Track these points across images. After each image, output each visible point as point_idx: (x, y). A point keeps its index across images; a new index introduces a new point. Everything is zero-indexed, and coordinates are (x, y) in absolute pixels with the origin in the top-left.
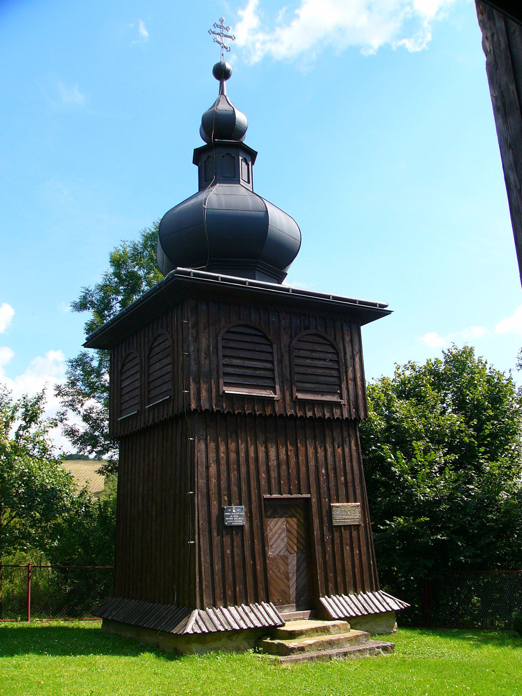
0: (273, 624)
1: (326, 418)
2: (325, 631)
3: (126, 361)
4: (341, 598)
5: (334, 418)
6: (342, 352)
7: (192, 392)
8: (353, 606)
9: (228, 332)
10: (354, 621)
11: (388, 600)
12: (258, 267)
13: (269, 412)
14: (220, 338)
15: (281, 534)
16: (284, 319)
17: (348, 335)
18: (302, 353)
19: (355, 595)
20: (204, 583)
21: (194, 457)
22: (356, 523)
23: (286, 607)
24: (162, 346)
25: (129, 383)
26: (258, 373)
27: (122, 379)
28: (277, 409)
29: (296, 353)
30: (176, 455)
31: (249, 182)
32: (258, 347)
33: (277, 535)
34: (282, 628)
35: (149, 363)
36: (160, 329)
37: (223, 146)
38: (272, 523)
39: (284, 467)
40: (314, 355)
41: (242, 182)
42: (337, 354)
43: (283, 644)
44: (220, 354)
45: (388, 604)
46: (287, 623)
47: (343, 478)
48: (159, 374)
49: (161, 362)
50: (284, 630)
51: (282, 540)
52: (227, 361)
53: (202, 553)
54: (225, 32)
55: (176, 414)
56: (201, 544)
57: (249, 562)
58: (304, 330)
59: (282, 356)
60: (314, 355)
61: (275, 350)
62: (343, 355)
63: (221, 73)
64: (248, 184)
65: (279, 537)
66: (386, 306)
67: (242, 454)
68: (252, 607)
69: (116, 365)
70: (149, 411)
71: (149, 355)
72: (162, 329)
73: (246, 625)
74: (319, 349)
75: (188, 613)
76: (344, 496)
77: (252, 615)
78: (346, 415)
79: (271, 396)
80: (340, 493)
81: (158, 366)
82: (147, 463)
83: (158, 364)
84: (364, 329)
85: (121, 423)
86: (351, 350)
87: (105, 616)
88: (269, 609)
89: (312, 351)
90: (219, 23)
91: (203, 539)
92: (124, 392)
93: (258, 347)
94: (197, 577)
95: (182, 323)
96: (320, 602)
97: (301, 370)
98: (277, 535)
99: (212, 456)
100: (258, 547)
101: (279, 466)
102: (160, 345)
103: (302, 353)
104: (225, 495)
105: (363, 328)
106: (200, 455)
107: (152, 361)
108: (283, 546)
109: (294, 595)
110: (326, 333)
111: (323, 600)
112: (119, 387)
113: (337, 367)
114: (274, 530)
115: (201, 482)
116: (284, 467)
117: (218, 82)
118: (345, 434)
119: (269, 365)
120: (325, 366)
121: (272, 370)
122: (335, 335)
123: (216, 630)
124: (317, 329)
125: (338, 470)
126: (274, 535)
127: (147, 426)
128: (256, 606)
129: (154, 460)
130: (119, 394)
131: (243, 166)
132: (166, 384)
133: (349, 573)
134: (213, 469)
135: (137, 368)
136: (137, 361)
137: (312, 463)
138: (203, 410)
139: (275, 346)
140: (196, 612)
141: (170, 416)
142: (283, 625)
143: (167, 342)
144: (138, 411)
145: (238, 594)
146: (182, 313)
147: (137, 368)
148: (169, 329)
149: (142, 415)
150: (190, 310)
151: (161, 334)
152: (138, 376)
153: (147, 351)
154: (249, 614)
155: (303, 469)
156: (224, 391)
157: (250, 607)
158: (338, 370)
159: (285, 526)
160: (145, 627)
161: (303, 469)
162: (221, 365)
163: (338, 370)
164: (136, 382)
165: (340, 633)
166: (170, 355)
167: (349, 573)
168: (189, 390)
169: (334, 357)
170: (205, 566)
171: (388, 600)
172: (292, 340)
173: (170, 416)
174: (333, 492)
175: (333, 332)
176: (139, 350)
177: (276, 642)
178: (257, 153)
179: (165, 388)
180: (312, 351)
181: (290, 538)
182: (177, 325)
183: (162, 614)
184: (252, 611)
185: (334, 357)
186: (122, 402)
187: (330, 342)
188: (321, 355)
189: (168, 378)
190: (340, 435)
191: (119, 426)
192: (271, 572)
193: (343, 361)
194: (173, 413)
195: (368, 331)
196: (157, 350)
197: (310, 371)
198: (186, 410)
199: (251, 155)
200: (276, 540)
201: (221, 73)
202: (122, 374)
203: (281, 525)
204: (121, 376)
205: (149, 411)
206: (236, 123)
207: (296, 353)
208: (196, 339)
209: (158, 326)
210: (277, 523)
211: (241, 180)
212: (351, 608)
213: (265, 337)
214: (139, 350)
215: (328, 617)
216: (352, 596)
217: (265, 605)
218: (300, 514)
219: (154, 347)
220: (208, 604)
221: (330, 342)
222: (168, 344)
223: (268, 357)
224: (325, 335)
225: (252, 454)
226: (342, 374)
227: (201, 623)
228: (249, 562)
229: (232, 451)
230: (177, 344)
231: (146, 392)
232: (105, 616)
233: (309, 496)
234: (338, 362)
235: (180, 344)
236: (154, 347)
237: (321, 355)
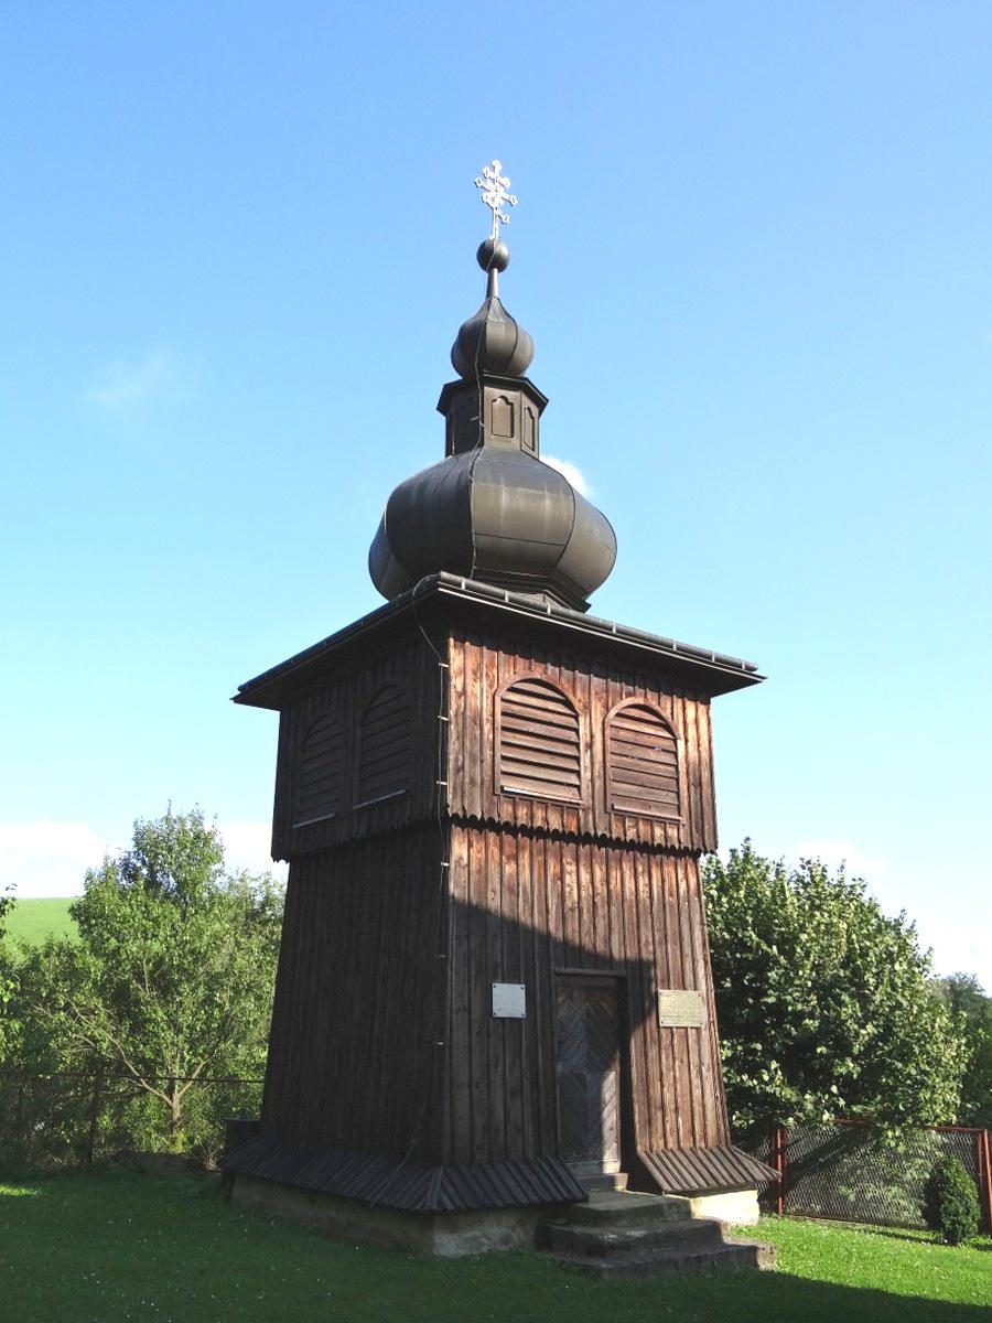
3: (315, 729)
9: (512, 690)
14: (498, 699)
31: (533, 450)
34: (580, 1205)
37: (484, 369)
58: (446, 781)
63: (490, 259)
66: (755, 670)
109: (605, 1113)
110: (659, 704)
117: (485, 275)
139: (581, 719)
140: (441, 1172)
141: (404, 824)
156: (502, 787)
169: (668, 744)
172: (608, 712)
177: (578, 1230)
178: (548, 400)
185: (668, 744)
187: (562, 694)
194: (410, 819)
201: (490, 259)
213: (568, 704)
221: (562, 694)
224: (657, 708)
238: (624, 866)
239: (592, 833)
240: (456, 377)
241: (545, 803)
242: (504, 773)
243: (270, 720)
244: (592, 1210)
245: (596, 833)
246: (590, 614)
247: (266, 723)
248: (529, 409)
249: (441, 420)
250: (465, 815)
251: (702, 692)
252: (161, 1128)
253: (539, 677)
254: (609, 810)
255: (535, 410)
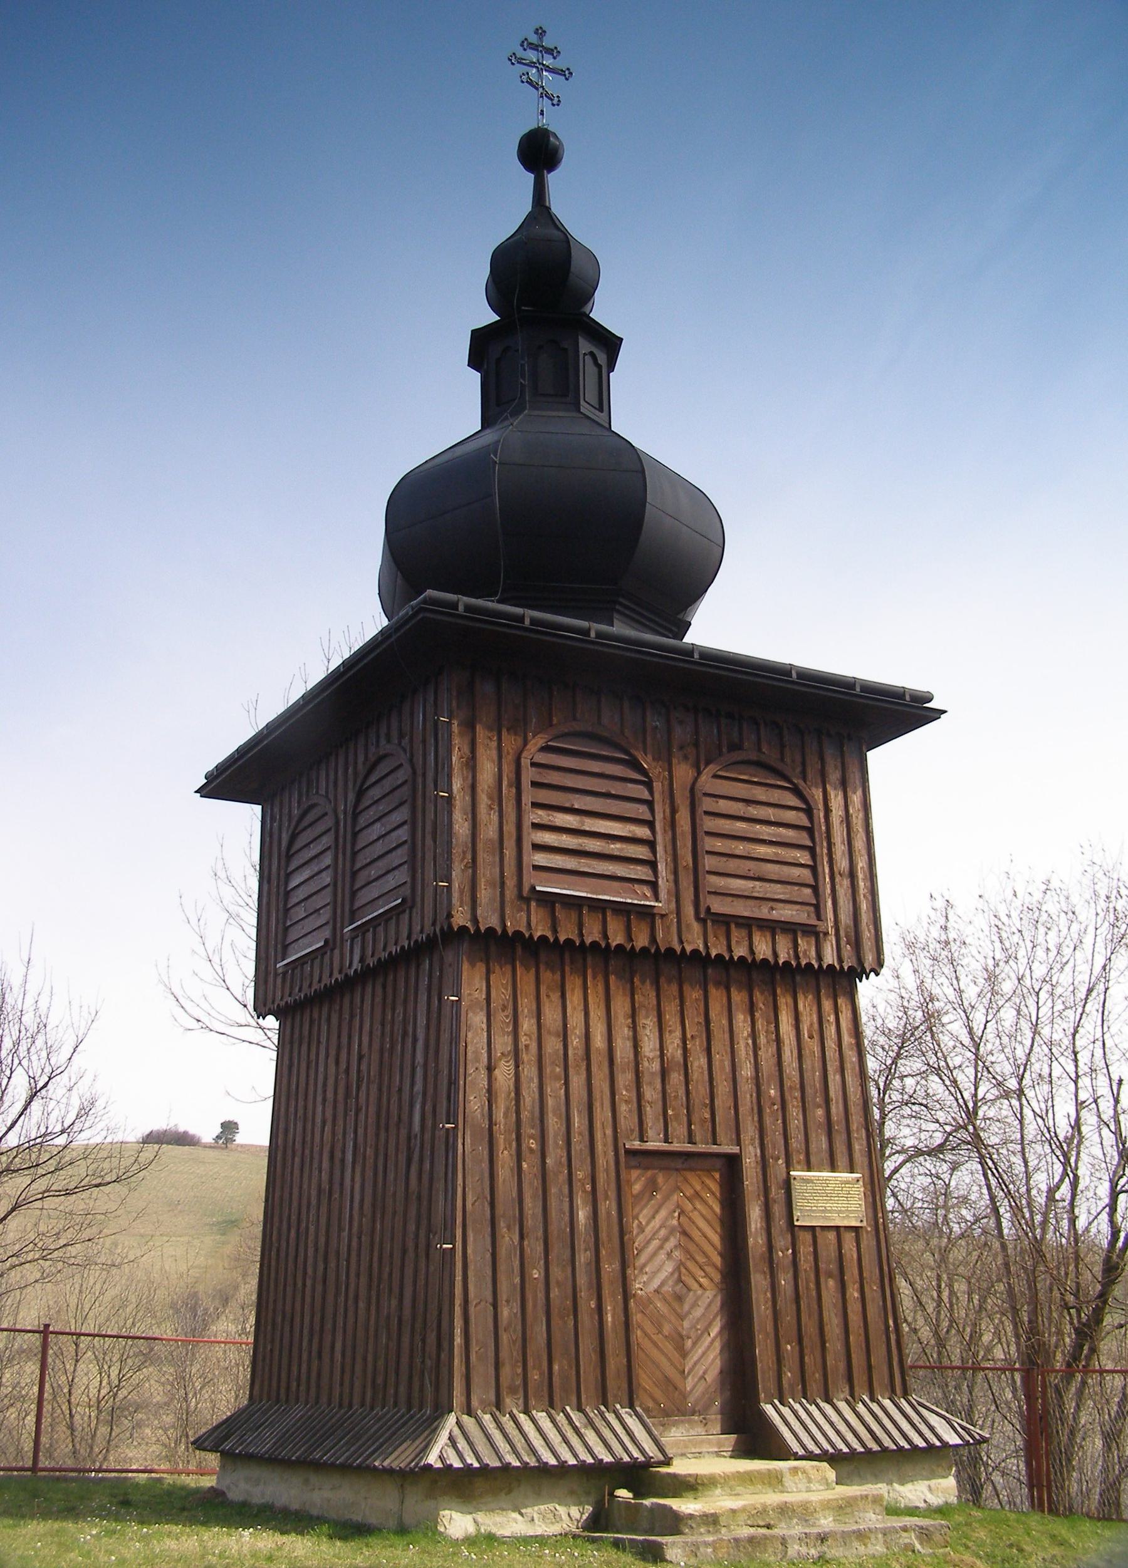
0: (642, 1459)
1: (781, 962)
2: (774, 1482)
4: (812, 1409)
5: (799, 964)
6: (821, 806)
7: (456, 885)
8: (842, 1427)
9: (546, 749)
10: (847, 1462)
11: (934, 1420)
12: (621, 604)
13: (641, 940)
14: (525, 762)
15: (666, 1239)
16: (681, 722)
17: (836, 767)
18: (723, 806)
19: (847, 1402)
20: (474, 1348)
21: (457, 1043)
22: (854, 1224)
23: (675, 1424)
24: (388, 784)
25: (307, 877)
26: (615, 848)
27: (290, 869)
28: (660, 935)
29: (708, 804)
30: (415, 1040)
32: (616, 788)
33: (655, 1243)
34: (664, 1470)
35: (352, 885)
36: (383, 741)
38: (645, 1211)
39: (676, 1078)
40: (754, 811)
41: (585, 408)
42: (809, 812)
43: (664, 1506)
44: (527, 799)
45: (932, 1429)
46: (675, 1462)
47: (820, 1112)
48: (379, 848)
49: (384, 820)
50: (669, 1474)
51: (669, 1255)
52: (542, 816)
53: (470, 1273)
54: (548, 61)
55: (416, 941)
56: (469, 1251)
57: (588, 1303)
59: (674, 811)
60: (754, 811)
61: (657, 796)
62: (822, 815)
64: (597, 412)
65: (661, 1247)
67: (575, 1042)
68: (591, 1415)
69: (276, 837)
70: (353, 940)
71: (356, 806)
72: (389, 741)
73: (575, 1456)
74: (763, 798)
75: (430, 1426)
76: (825, 1155)
77: (591, 1436)
78: (830, 958)
79: (648, 903)
80: (813, 1147)
81: (377, 829)
82: (343, 1066)
83: (378, 825)
84: (876, 758)
85: (285, 974)
86: (842, 803)
87: (227, 1446)
88: (632, 1422)
89: (748, 802)
90: (534, 39)
91: (475, 1240)
92: (294, 900)
93: (616, 788)
94: (458, 1331)
95: (436, 723)
96: (762, 1415)
97: (719, 845)
98: (655, 1243)
99: (503, 1043)
100: (610, 1268)
101: (664, 1073)
102: (384, 781)
103: (723, 806)
104: (531, 1137)
105: (871, 755)
106: (473, 1038)
107: (362, 821)
108: (670, 1270)
110: (782, 759)
111: (769, 1409)
112: (282, 888)
113: (809, 844)
114: (648, 1229)
115: (475, 1104)
116: (676, 1078)
117: (530, 177)
118: (827, 1005)
119: (643, 832)
120: (779, 840)
121: (651, 844)
122: (804, 764)
123: (498, 1464)
124: (760, 750)
125: (809, 1091)
126: (649, 1242)
127: (346, 975)
128: (602, 1414)
129: (360, 1058)
130: (281, 905)
131: (589, 371)
132: (396, 872)
133: (835, 1346)
134: (504, 1073)
135: (327, 840)
136: (328, 822)
137: (746, 1071)
138: (483, 929)
140: (452, 1419)
141: (403, 948)
142: (667, 1462)
143: (401, 772)
144: (326, 941)
145: (556, 1379)
146: (436, 699)
147: (327, 840)
148: (405, 741)
149: (337, 952)
150: (454, 694)
151: (385, 756)
152: (327, 860)
153: (351, 796)
154: (583, 1431)
155: (723, 1088)
156: (708, 909)
157: (586, 1415)
158: (812, 850)
159: (675, 1222)
160: (325, 1463)
161: (723, 1088)
162: (526, 825)
163: (812, 850)
164: (324, 874)
165: (809, 1490)
166: (405, 801)
167: (835, 1346)
168: (449, 879)
170: (481, 1315)
171: (934, 1420)
173: (403, 948)
174: (796, 1143)
175: (798, 758)
176: (331, 797)
179: (391, 881)
180: (748, 802)
181: (687, 1251)
182: (424, 729)
183: (369, 1429)
184: (591, 1423)
186: (289, 924)
188: (770, 813)
189: (400, 856)
190: (815, 1008)
191: (279, 980)
192: (639, 1332)
193: (823, 828)
194: (409, 937)
195: (885, 762)
196: (376, 793)
197: (741, 848)
198: (442, 929)
199: (611, 344)
200: (655, 1254)
202: (289, 857)
203: (666, 1219)
204: (287, 866)
205: (353, 940)
206: (572, 269)
207: (708, 804)
208: (471, 764)
209: (378, 737)
210: (657, 1212)
211: (582, 402)
212: (838, 1432)
214: (331, 797)
215: (783, 1453)
216: (842, 1405)
217: (624, 1412)
218: (713, 1193)
219: (368, 788)
220: (482, 1402)
222: (401, 776)
223: (642, 811)
224: (779, 766)
225: (599, 1041)
226: (818, 859)
227: (462, 1444)
228: (588, 1303)
229: (549, 1032)
230: (424, 775)
231: (347, 896)
232: (227, 1446)
233: (735, 1150)
234: (810, 831)
235: (430, 775)
236: (368, 788)
237: (770, 813)
238: (839, 1001)
239: (678, 949)
240: (490, 317)
241: (599, 907)
242: (536, 868)
243: (243, 821)
244: (674, 1476)
245: (683, 949)
246: (692, 637)
247: (243, 821)
248: (592, 354)
249: (474, 378)
250: (820, 966)
251: (850, 738)
252: (706, 1524)
253: (590, 729)
254: (707, 917)
255: (602, 358)
